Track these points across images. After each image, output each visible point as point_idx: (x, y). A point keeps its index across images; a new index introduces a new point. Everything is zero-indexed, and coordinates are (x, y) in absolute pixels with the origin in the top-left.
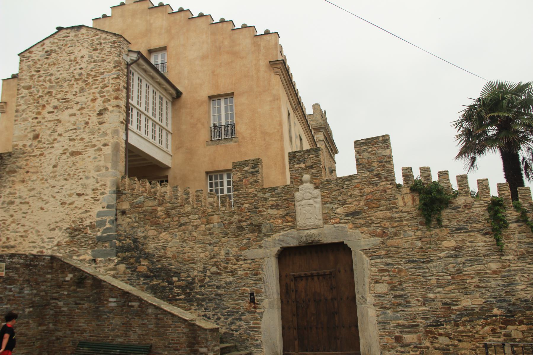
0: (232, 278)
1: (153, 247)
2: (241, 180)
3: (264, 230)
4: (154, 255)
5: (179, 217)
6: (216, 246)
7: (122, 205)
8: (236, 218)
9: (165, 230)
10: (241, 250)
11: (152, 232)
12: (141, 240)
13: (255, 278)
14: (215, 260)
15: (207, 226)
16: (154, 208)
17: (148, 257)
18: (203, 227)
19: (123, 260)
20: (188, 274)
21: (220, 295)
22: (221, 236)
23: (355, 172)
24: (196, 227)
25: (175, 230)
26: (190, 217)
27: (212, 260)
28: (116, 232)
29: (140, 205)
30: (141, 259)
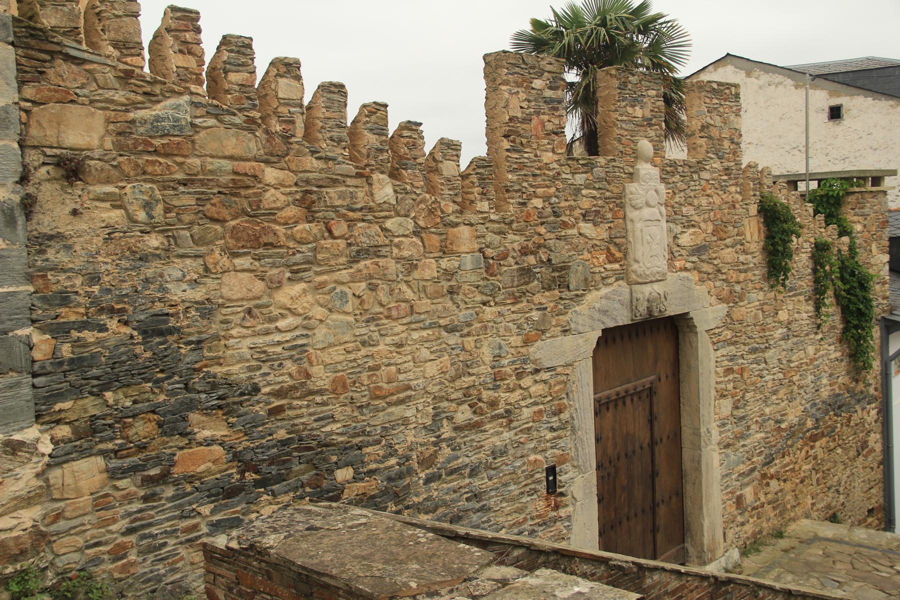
0: (507, 435)
1: (247, 353)
2: (527, 120)
3: (574, 280)
4: (256, 389)
5: (351, 223)
6: (468, 334)
7: (59, 122)
8: (514, 241)
9: (296, 275)
10: (527, 342)
11: (238, 284)
12: (190, 324)
13: (555, 421)
14: (467, 380)
15: (444, 263)
16: (246, 166)
17: (228, 399)
18: (429, 269)
19: (87, 437)
20: (390, 446)
21: (476, 496)
22: (479, 298)
23: (454, 115)
24: (411, 265)
25: (336, 276)
26: (389, 224)
27: (458, 384)
28: (30, 279)
29: (174, 142)
30: (194, 417)
